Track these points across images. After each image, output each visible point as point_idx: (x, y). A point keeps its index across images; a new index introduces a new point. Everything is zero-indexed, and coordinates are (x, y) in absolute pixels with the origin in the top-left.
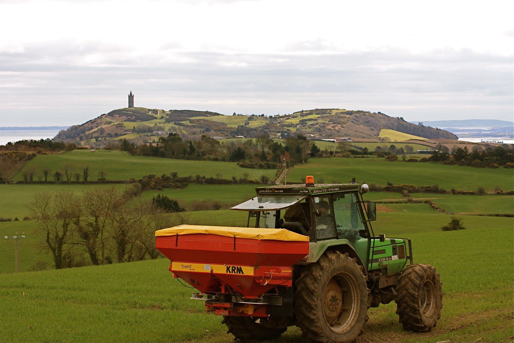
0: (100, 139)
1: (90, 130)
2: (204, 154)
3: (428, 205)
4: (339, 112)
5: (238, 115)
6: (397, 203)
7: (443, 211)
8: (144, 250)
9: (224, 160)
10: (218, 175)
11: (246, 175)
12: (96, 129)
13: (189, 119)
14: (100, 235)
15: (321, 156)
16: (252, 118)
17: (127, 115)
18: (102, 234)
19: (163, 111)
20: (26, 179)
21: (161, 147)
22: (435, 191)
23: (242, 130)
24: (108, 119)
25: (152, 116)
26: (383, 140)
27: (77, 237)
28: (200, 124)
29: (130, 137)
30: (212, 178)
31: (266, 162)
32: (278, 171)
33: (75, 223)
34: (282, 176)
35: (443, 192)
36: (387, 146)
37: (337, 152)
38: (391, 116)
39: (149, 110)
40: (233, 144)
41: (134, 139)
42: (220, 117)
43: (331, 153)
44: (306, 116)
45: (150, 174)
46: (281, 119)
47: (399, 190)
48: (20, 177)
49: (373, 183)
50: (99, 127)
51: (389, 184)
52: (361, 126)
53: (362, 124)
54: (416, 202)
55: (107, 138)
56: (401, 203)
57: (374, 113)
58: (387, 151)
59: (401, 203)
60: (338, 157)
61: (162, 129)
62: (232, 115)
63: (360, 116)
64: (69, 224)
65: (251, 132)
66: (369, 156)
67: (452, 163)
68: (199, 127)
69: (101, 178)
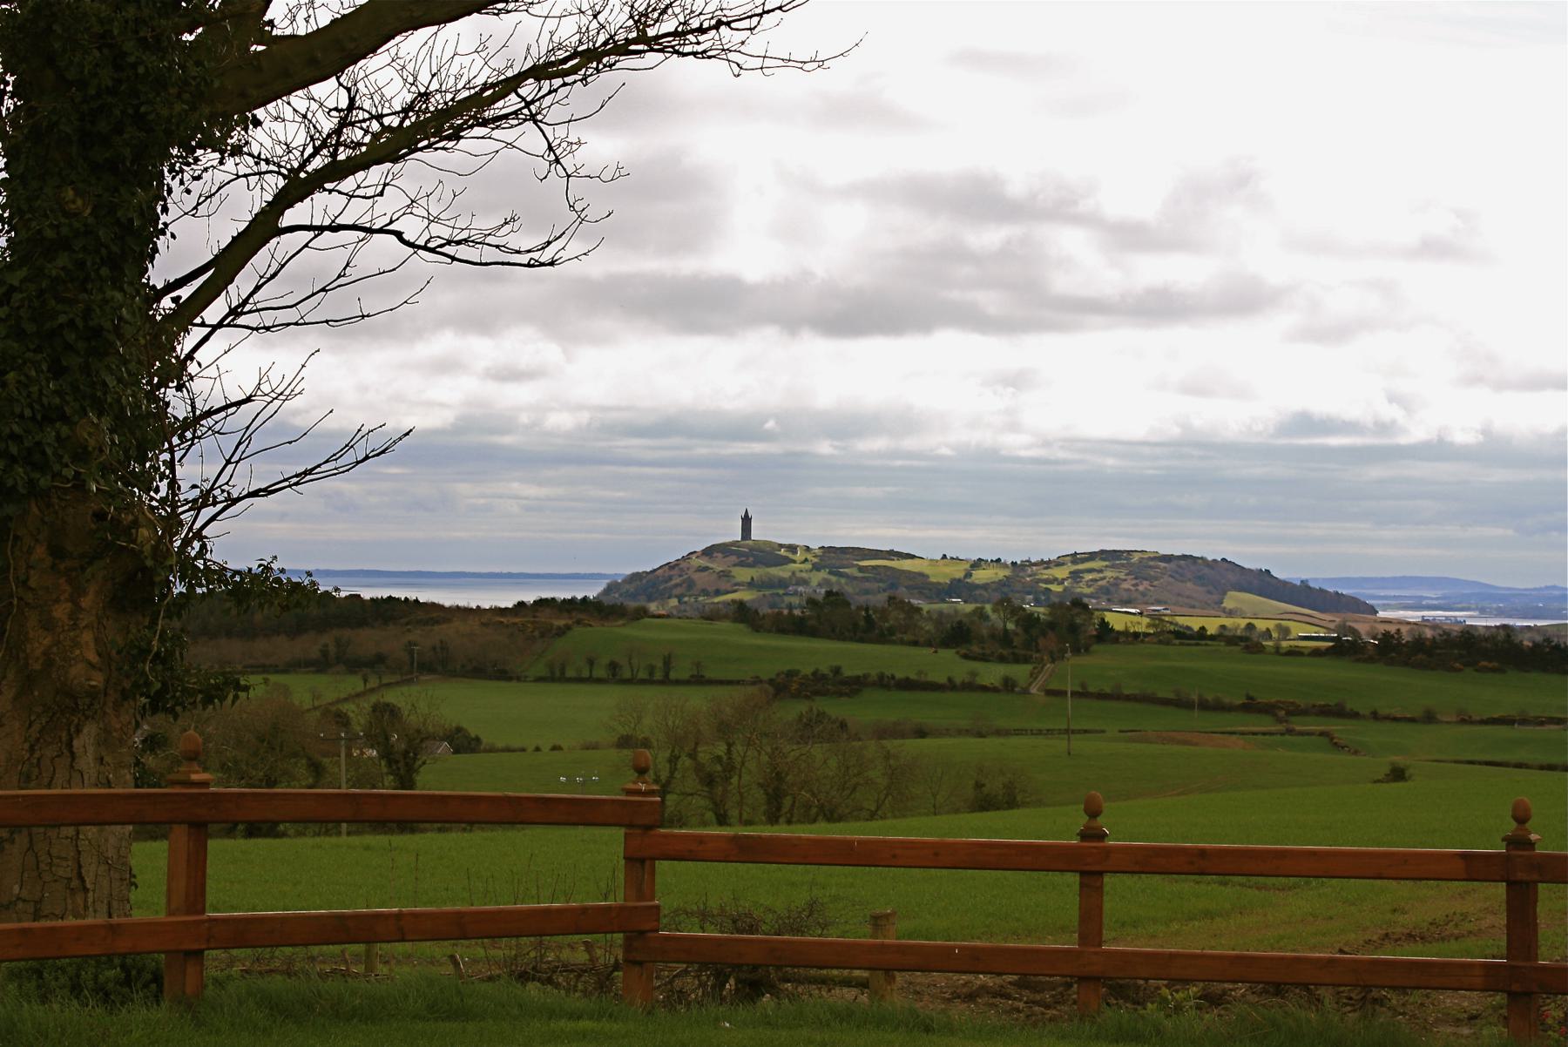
2: (891, 631)
3: (1324, 740)
6: (1264, 734)
7: (1356, 753)
8: (814, 810)
9: (929, 644)
11: (974, 674)
14: (735, 780)
15: (1116, 641)
16: (978, 564)
22: (1339, 712)
23: (959, 587)
24: (703, 562)
27: (692, 783)
29: (745, 596)
34: (1041, 679)
35: (1355, 715)
37: (1146, 635)
38: (1246, 566)
39: (781, 546)
40: (941, 613)
42: (916, 561)
43: (1136, 635)
47: (1268, 709)
52: (1189, 585)
54: (1301, 734)
56: (1271, 734)
58: (1239, 633)
59: (1271, 734)
61: (805, 582)
62: (939, 557)
67: (1371, 660)
68: (875, 580)
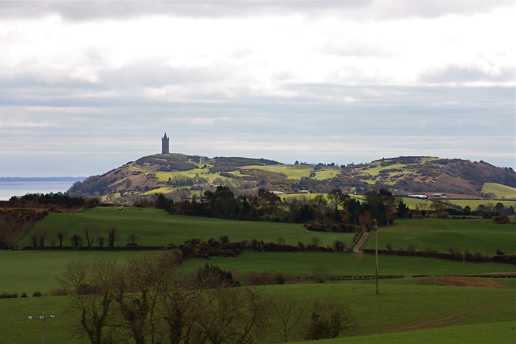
0: (126, 193)
1: (113, 182)
2: (261, 212)
4: (430, 160)
5: (302, 164)
6: (509, 277)
8: (203, 335)
10: (280, 239)
11: (316, 240)
12: (121, 181)
13: (239, 169)
14: (149, 315)
16: (320, 167)
17: (161, 164)
18: (152, 313)
19: (206, 159)
20: (35, 244)
21: (207, 204)
23: (305, 184)
24: (136, 169)
25: (193, 165)
26: (487, 197)
28: (253, 176)
29: (164, 190)
30: (272, 244)
31: (340, 224)
32: (356, 235)
33: (117, 300)
34: (361, 242)
36: (492, 204)
37: (430, 212)
38: (496, 166)
39: (189, 157)
40: (295, 200)
41: (170, 194)
43: (424, 213)
44: (388, 165)
45: (193, 238)
46: (356, 169)
48: (27, 241)
49: (479, 251)
50: (125, 179)
51: (499, 253)
53: (459, 176)
55: (136, 193)
57: (475, 162)
60: (432, 217)
62: (293, 163)
63: (457, 166)
64: (110, 301)
65: (319, 185)
66: (472, 217)
69: (131, 242)
